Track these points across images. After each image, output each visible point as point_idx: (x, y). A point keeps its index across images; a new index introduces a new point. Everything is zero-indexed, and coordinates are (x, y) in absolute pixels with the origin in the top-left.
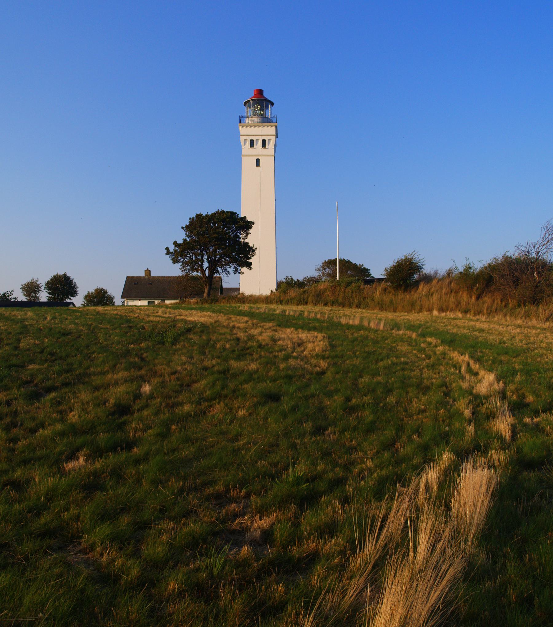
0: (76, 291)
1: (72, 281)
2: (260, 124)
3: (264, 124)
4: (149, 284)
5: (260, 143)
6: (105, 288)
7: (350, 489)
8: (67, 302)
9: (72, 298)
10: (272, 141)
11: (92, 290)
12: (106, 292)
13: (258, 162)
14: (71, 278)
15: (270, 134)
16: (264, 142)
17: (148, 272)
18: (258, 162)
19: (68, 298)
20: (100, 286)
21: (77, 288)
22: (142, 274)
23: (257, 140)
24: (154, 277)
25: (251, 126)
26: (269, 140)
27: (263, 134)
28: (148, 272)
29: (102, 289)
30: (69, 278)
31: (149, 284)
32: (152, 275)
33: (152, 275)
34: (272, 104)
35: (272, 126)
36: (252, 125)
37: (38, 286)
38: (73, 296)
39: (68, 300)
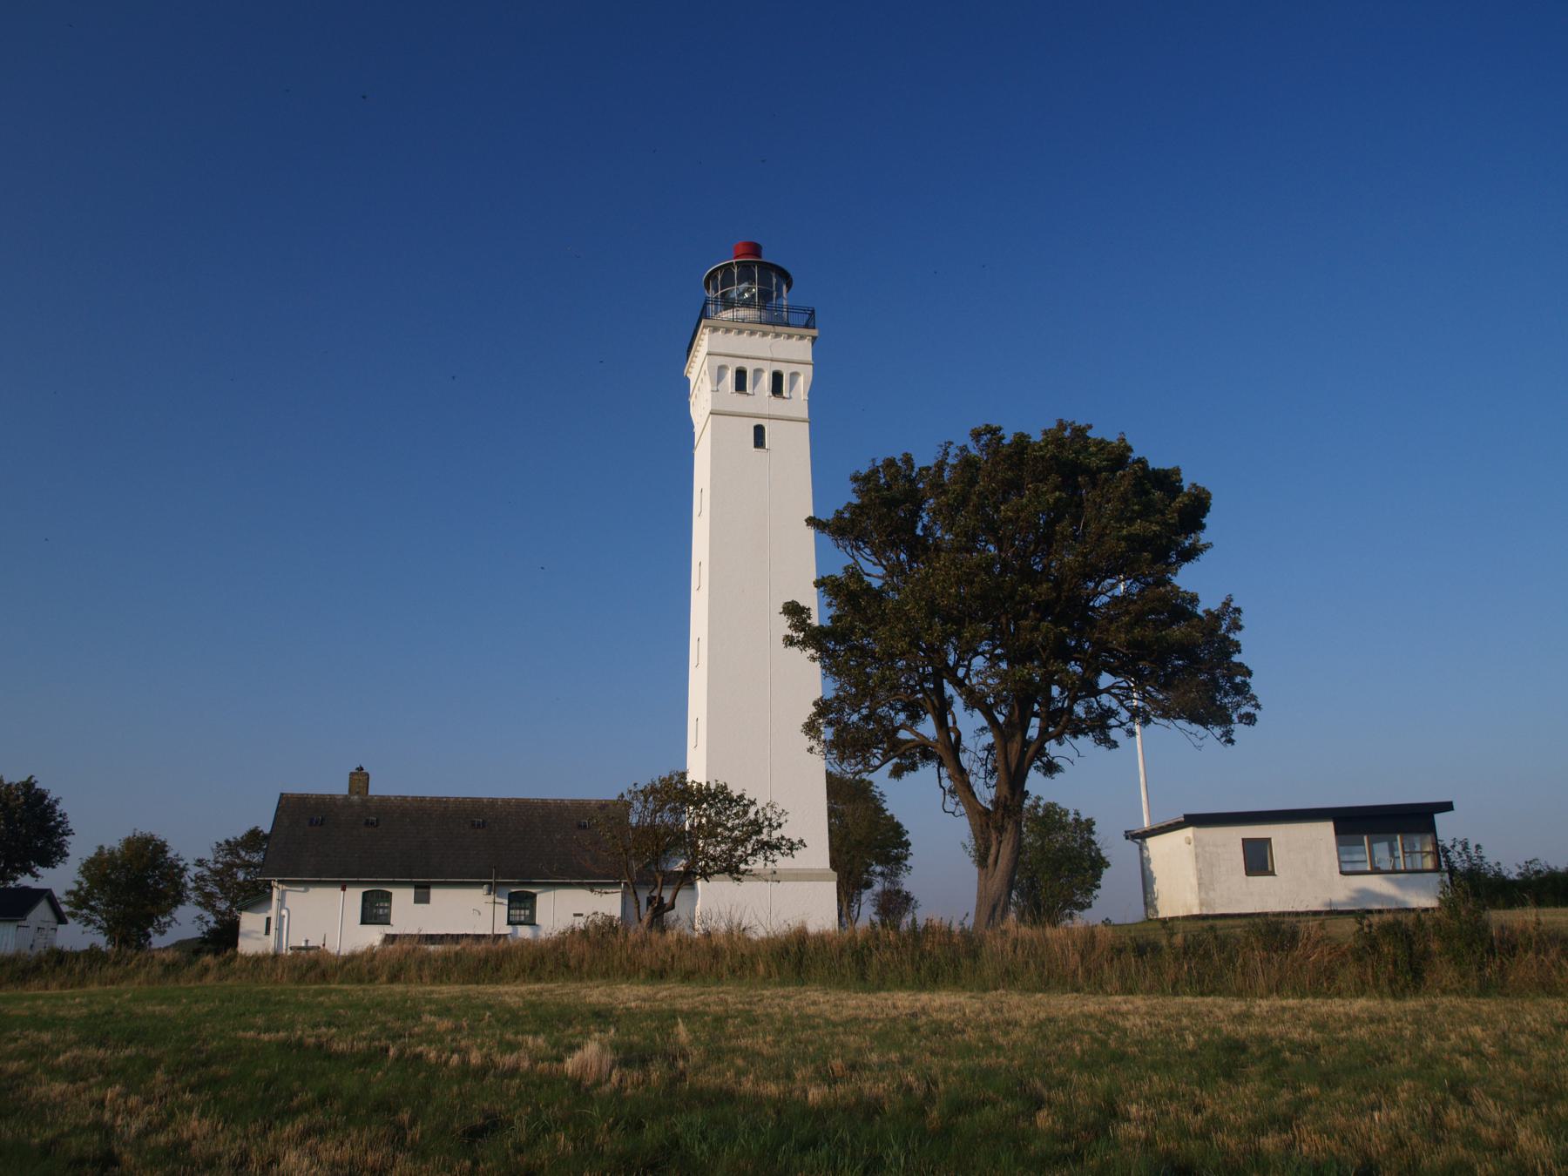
0: (60, 846)
1: (51, 807)
2: (769, 328)
3: (779, 329)
4: (367, 823)
5: (766, 379)
6: (161, 835)
7: (225, 1094)
8: (26, 889)
9: (41, 870)
10: (801, 380)
11: (113, 840)
12: (161, 848)
13: (759, 433)
14: (52, 796)
15: (795, 358)
16: (777, 378)
17: (360, 778)
18: (759, 433)
19: (28, 870)
20: (145, 828)
21: (69, 832)
22: (340, 788)
23: (758, 372)
24: (384, 800)
25: (728, 331)
26: (794, 375)
27: (776, 356)
28: (360, 778)
29: (148, 840)
30: (42, 796)
31: (367, 823)
32: (376, 789)
33: (376, 789)
34: (785, 276)
35: (802, 337)
36: (730, 325)
37: (173, 872)
38: (47, 862)
39: (25, 880)
